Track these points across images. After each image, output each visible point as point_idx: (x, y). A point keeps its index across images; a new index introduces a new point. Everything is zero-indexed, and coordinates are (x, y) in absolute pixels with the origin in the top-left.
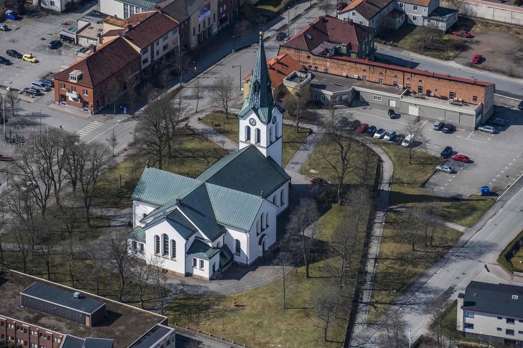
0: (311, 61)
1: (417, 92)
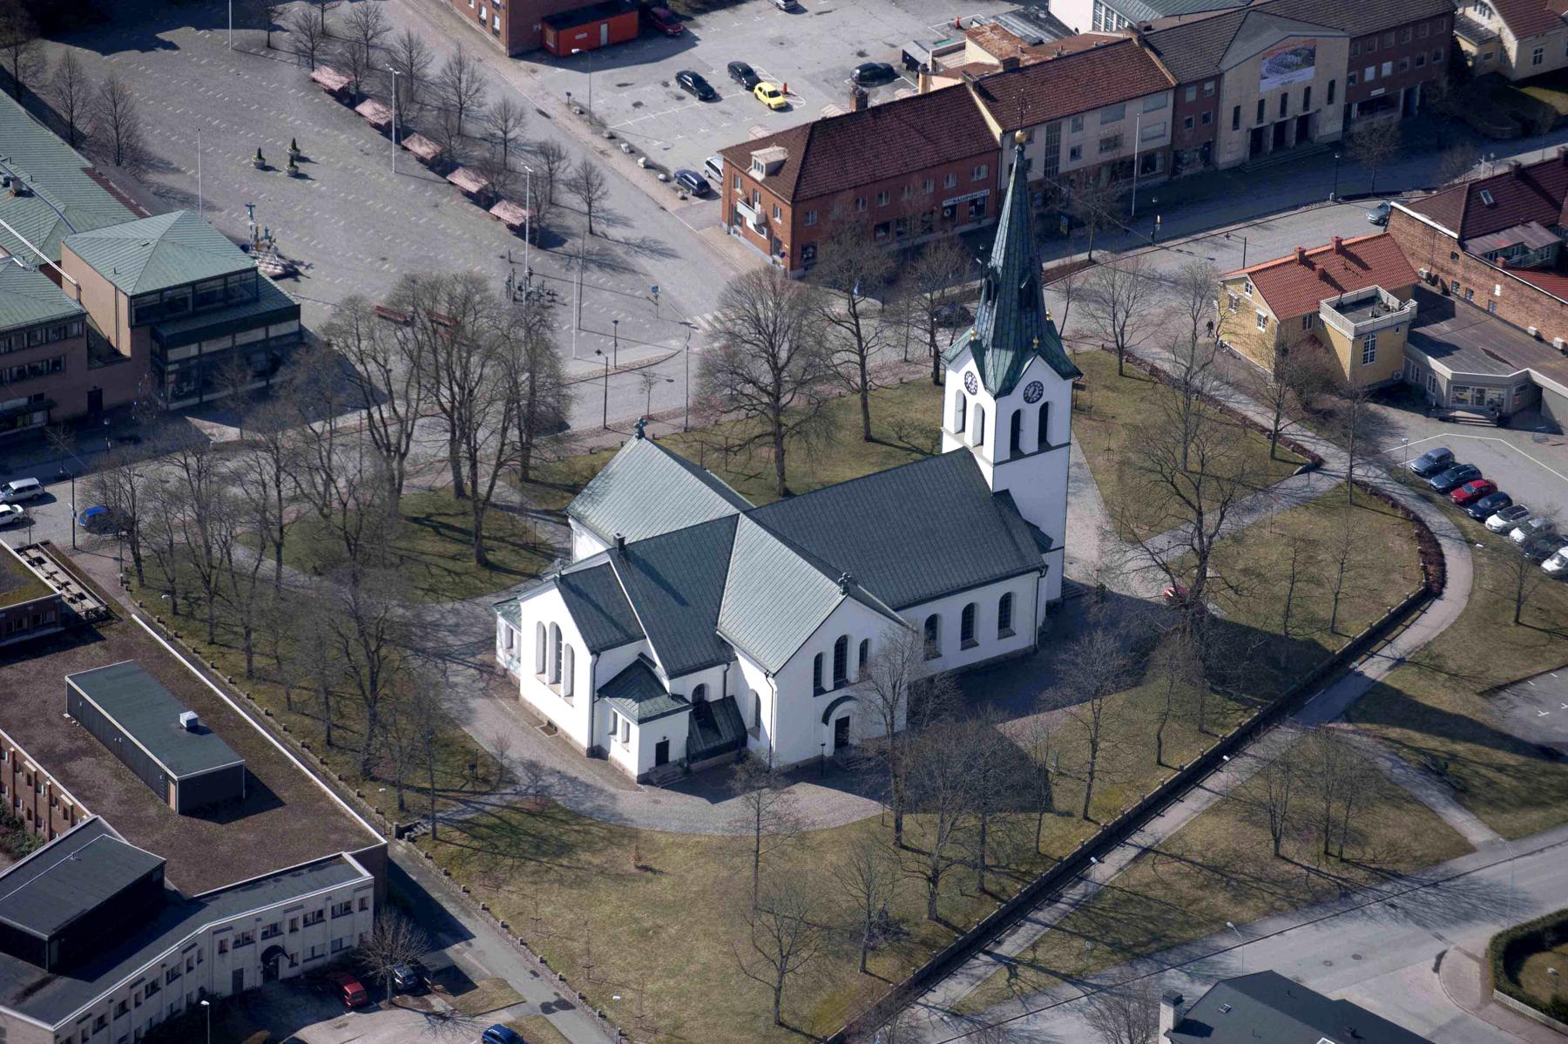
0: (1458, 269)
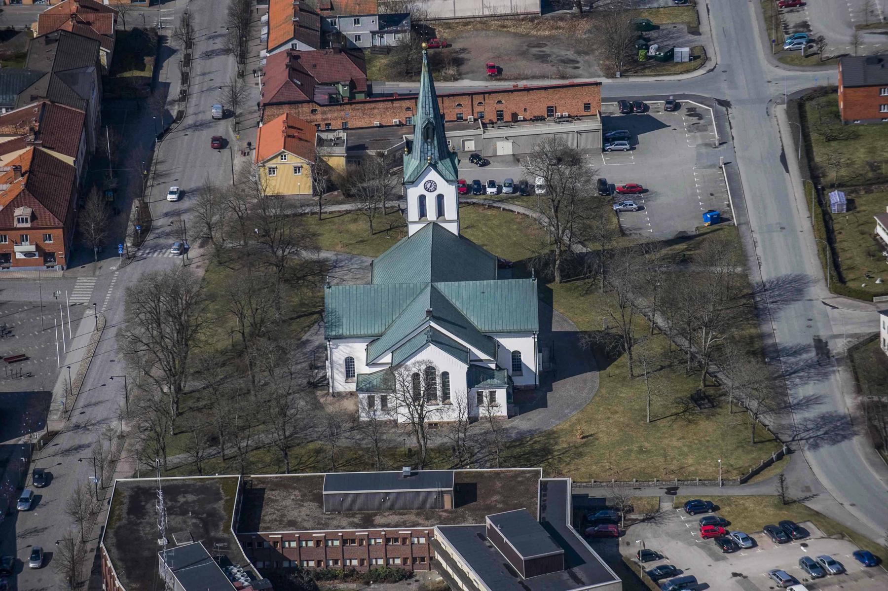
0: (318, 117)
1: (495, 120)
